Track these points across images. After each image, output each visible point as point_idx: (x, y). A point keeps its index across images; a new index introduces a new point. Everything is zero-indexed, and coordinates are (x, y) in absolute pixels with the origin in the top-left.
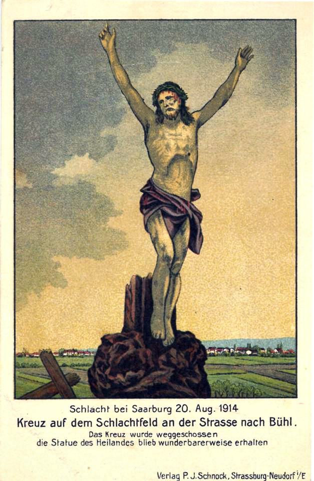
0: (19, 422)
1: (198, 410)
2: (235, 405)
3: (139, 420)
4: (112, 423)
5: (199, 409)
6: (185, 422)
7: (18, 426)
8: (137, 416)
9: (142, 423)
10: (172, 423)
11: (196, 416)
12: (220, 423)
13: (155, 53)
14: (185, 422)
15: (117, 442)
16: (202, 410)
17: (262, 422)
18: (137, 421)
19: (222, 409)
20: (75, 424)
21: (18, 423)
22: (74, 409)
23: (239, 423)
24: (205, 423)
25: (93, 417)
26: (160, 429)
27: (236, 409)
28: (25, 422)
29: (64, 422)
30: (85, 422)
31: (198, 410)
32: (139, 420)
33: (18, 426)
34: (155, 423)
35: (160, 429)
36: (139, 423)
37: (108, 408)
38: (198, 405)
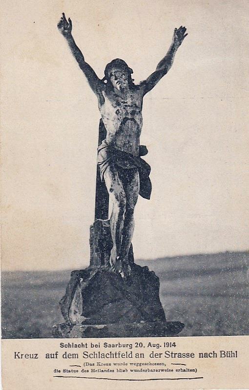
0: (16, 355)
1: (150, 346)
2: (174, 343)
3: (117, 353)
4: (96, 355)
5: (151, 345)
6: (154, 355)
7: (187, 34)
8: (107, 350)
9: (120, 355)
10: (142, 355)
11: (147, 351)
12: (182, 356)
13: (172, 61)
14: (154, 355)
15: (66, 358)
16: (152, 345)
17: (215, 355)
18: (116, 354)
19: (166, 345)
20: (65, 356)
21: (15, 356)
22: (62, 345)
23: (197, 356)
24: (153, 355)
25: (80, 351)
26: (134, 360)
27: (175, 346)
28: (22, 355)
29: (56, 354)
30: (73, 354)
31: (150, 346)
32: (117, 353)
33: (187, 34)
34: (130, 356)
35: (134, 360)
36: (117, 355)
37: (86, 345)
38: (150, 343)
